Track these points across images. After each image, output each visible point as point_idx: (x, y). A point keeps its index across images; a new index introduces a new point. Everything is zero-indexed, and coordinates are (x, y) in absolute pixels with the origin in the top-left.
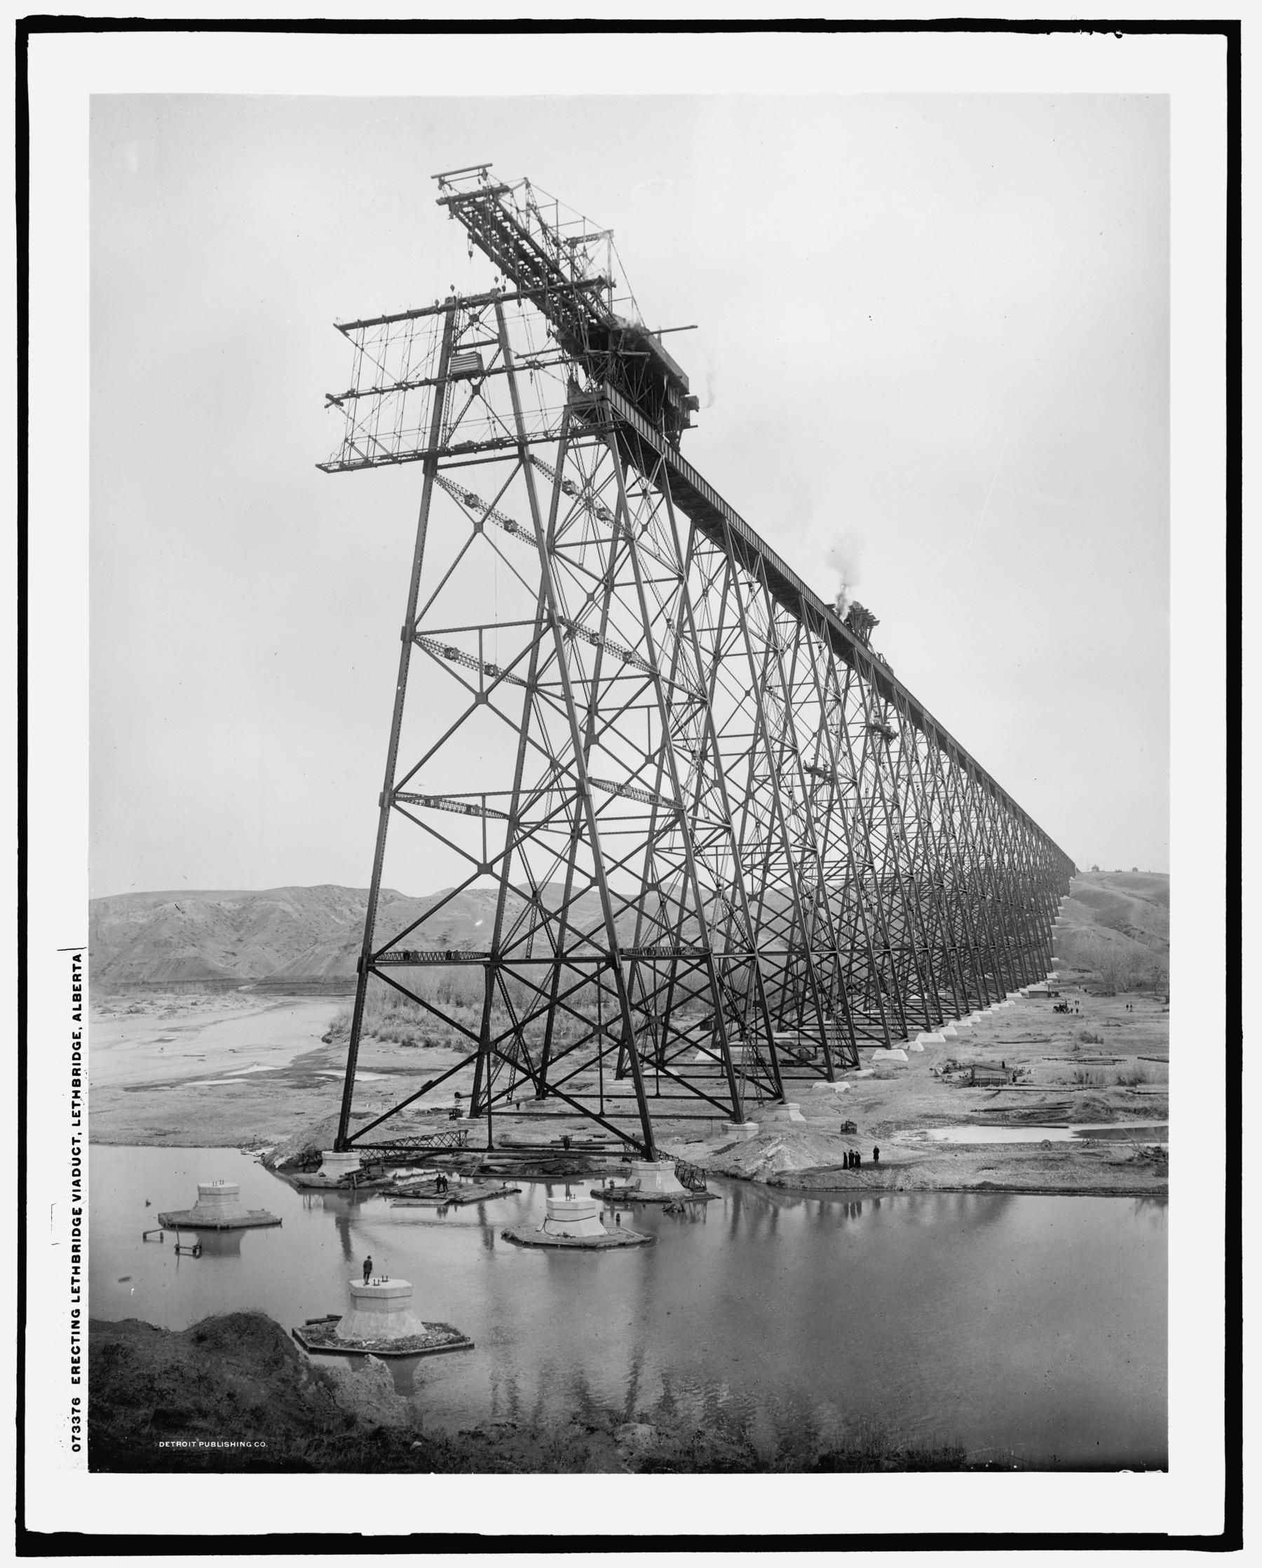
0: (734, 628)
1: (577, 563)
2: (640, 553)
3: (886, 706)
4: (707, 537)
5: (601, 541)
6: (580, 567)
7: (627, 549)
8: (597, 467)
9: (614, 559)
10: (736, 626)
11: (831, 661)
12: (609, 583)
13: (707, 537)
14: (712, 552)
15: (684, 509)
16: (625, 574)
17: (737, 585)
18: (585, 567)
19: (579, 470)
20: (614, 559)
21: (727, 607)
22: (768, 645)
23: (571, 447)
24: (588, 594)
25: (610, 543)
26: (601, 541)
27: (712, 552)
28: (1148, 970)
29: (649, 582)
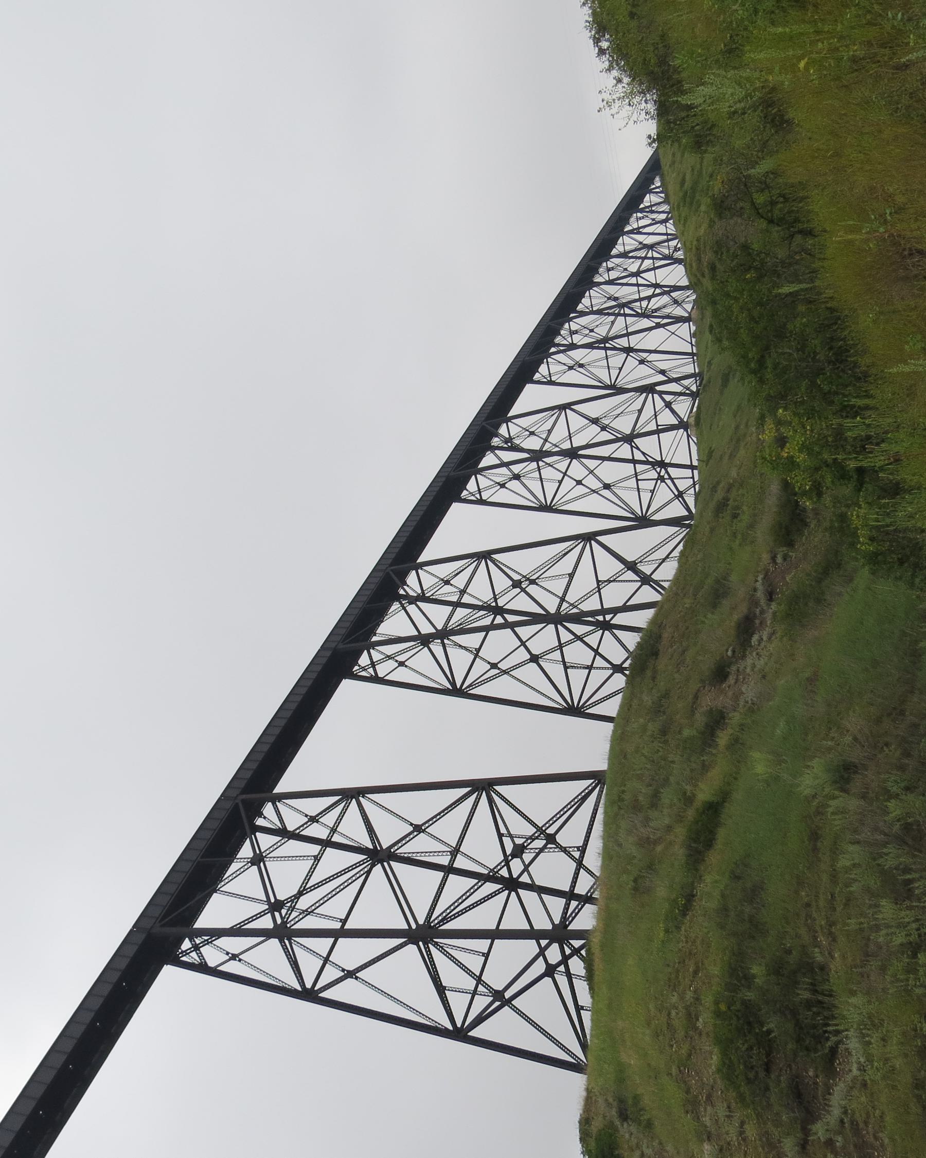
0: (666, 227)
1: (618, 371)
2: (611, 334)
3: (559, 345)
4: (615, 247)
5: (607, 356)
6: (621, 369)
7: (610, 342)
8: (560, 362)
9: (614, 348)
10: (666, 226)
11: (624, 255)
12: (628, 350)
13: (615, 247)
14: (590, 296)
15: (414, 529)
16: (623, 342)
17: (639, 228)
18: (620, 366)
19: (565, 372)
20: (614, 348)
21: (655, 232)
22: (619, 314)
23: (551, 379)
24: (581, 481)
25: (608, 351)
26: (607, 356)
27: (590, 296)
28: (818, 490)
29: (627, 328)
